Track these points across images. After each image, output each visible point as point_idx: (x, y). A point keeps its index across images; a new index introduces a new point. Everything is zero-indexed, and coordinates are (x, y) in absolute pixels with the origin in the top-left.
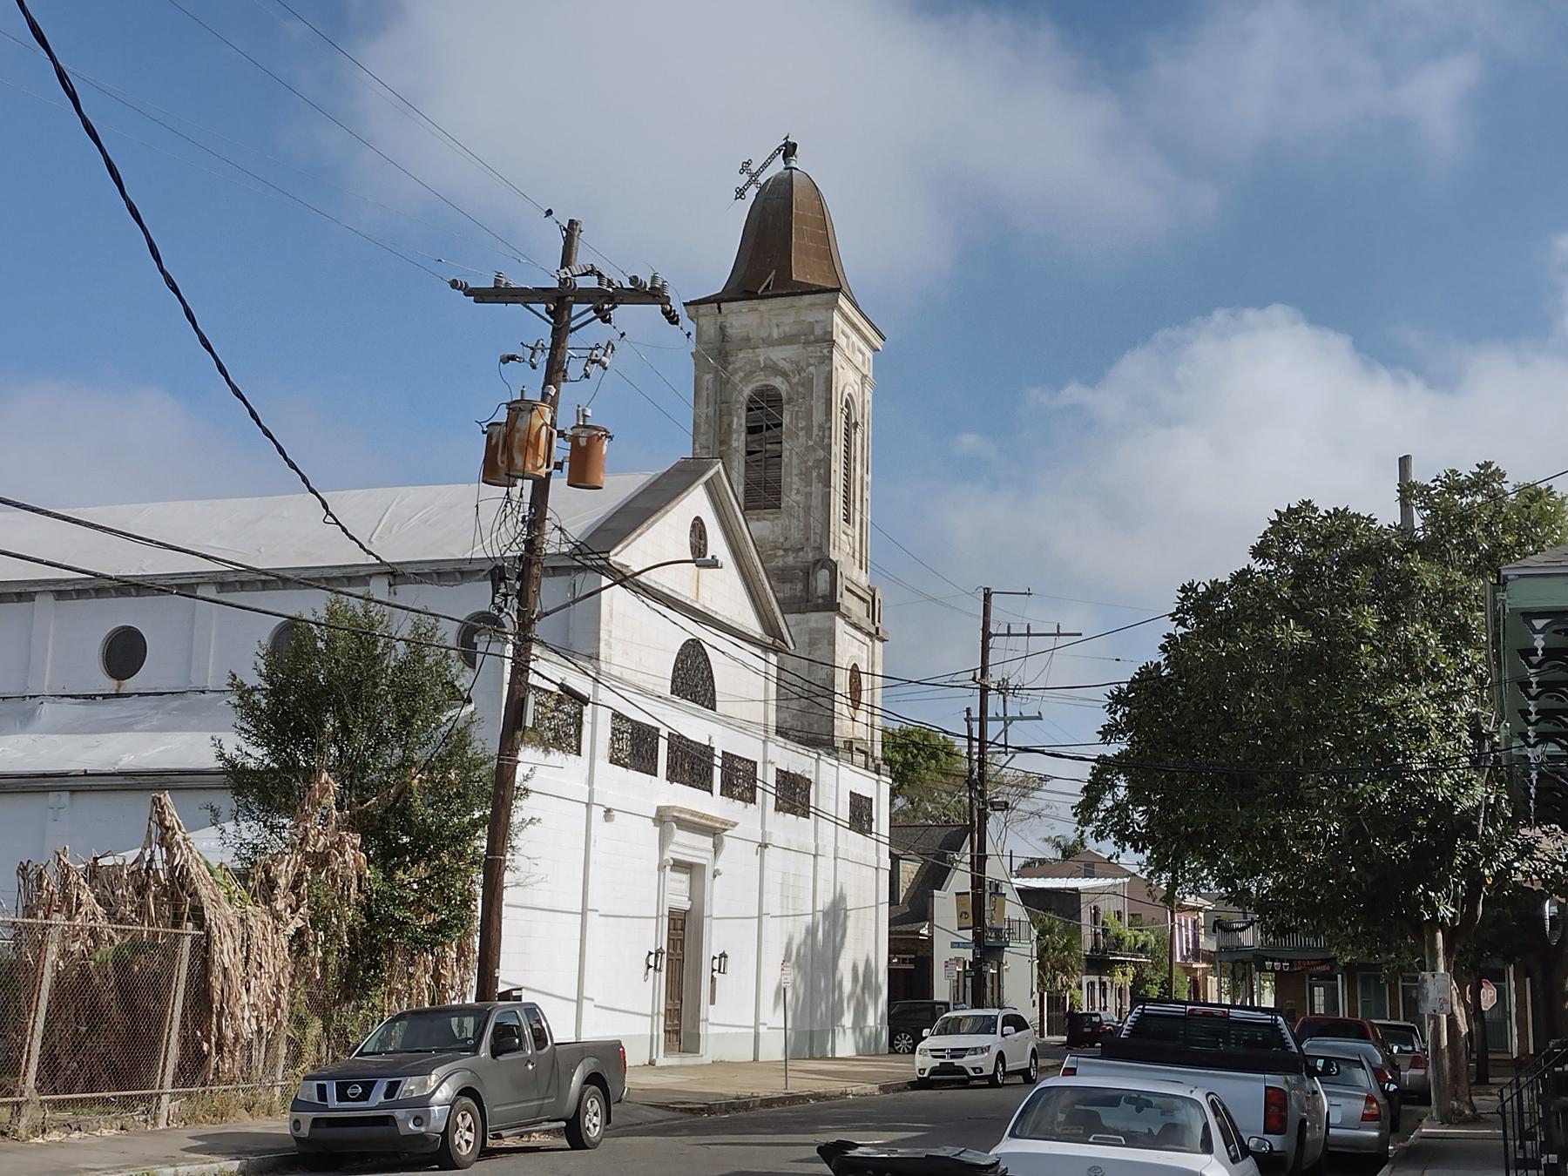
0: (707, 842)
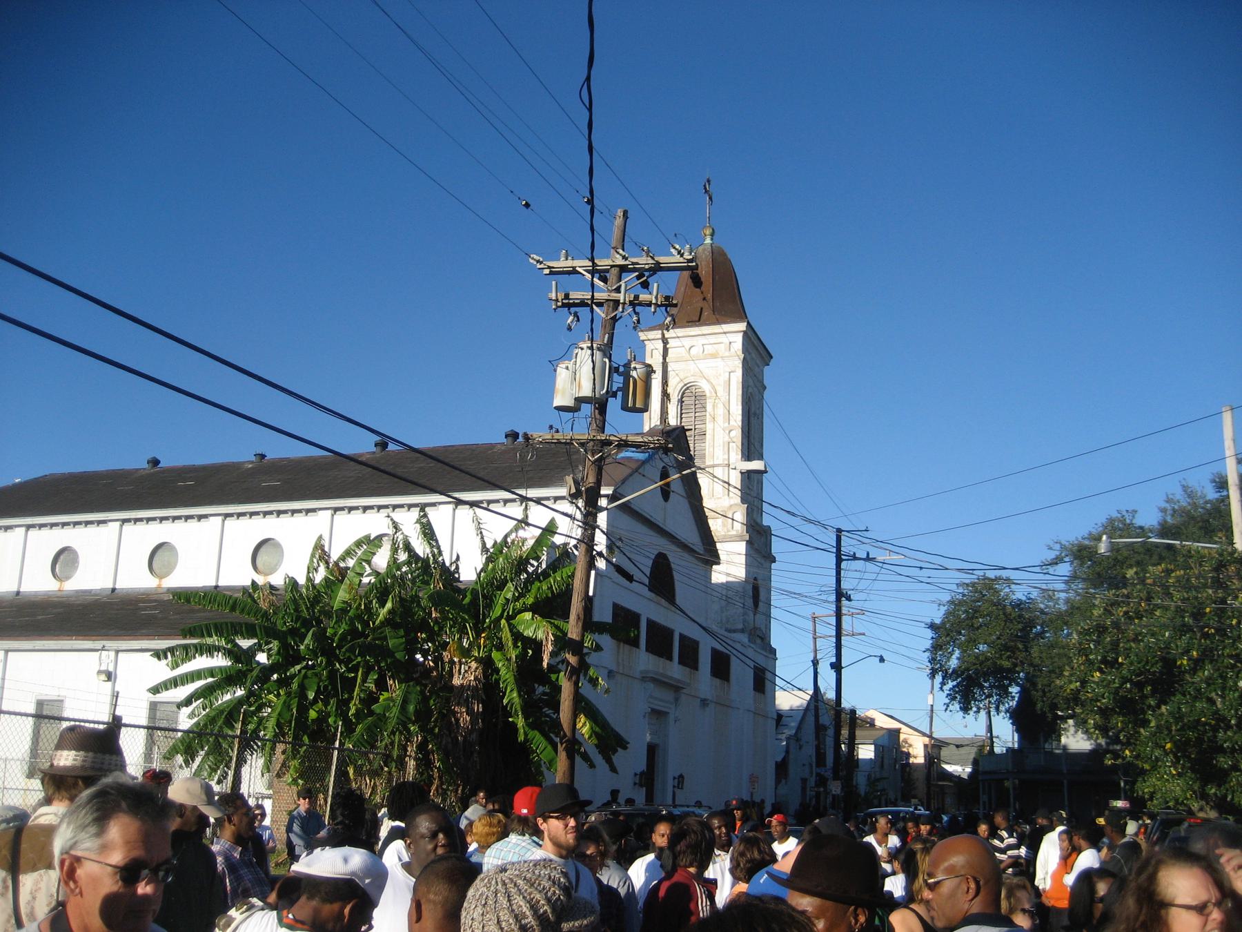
0: (669, 695)
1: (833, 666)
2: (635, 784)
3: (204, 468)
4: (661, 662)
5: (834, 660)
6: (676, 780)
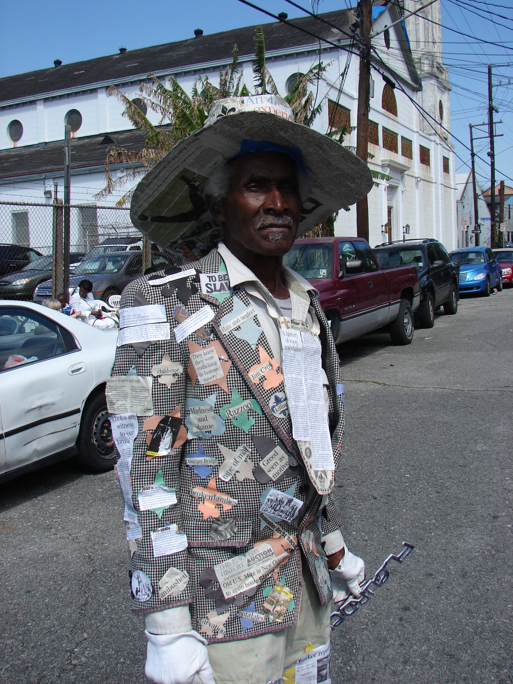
1: (489, 154)
2: (382, 232)
3: (89, 62)
4: (393, 154)
5: (489, 150)
6: (405, 228)
